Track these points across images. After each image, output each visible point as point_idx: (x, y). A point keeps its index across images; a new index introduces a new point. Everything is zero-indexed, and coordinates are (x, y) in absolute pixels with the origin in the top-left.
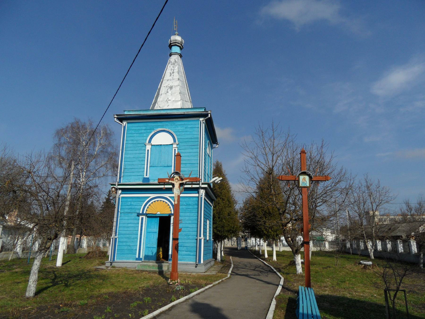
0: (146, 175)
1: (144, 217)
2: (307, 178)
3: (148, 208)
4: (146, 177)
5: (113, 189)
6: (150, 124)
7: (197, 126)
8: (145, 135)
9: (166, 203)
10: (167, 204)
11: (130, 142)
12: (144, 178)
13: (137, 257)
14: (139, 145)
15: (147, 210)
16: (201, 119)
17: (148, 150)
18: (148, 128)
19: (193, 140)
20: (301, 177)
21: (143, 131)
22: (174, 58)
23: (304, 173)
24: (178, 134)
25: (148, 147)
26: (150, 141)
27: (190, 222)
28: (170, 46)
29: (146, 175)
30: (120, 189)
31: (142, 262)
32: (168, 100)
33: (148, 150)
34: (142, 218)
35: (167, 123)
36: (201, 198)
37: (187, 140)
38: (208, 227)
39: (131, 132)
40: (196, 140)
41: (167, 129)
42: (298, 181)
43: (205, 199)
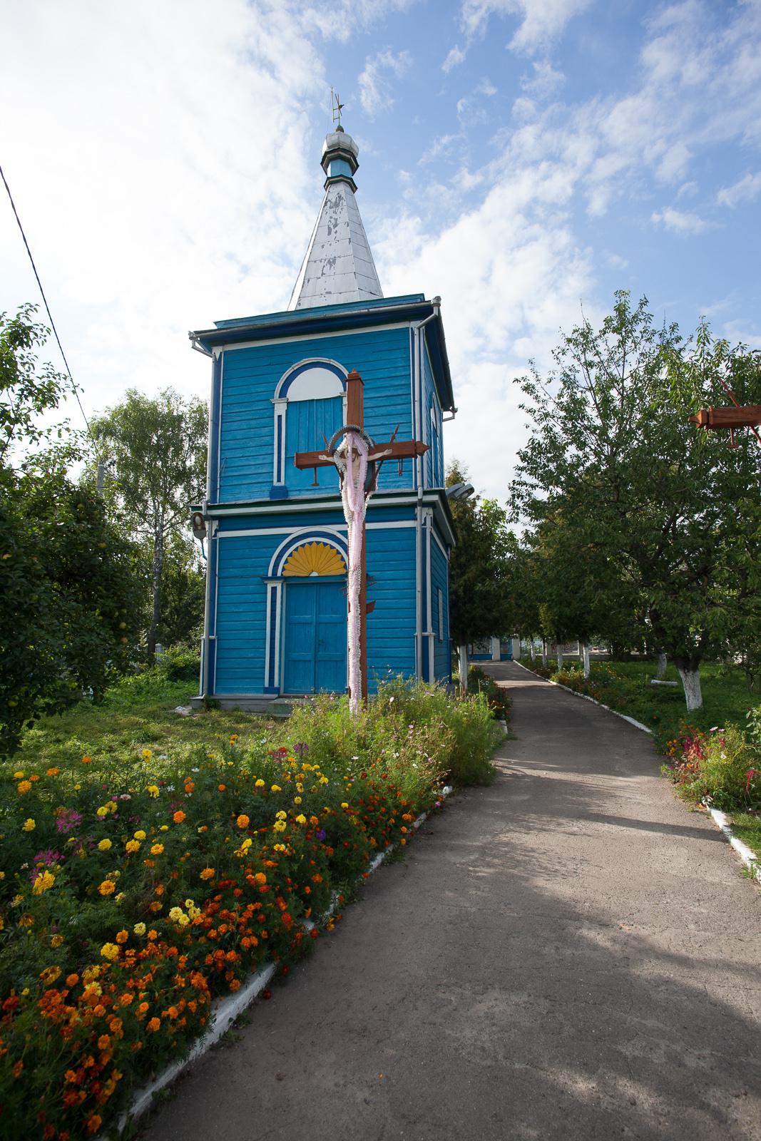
0: (279, 480)
3: (286, 562)
4: (279, 484)
5: (197, 518)
9: (332, 547)
10: (334, 551)
13: (267, 685)
15: (284, 569)
16: (415, 325)
17: (280, 417)
25: (281, 409)
26: (283, 394)
29: (279, 480)
30: (214, 518)
31: (279, 697)
33: (280, 417)
34: (274, 589)
36: (424, 531)
38: (441, 618)
43: (431, 533)
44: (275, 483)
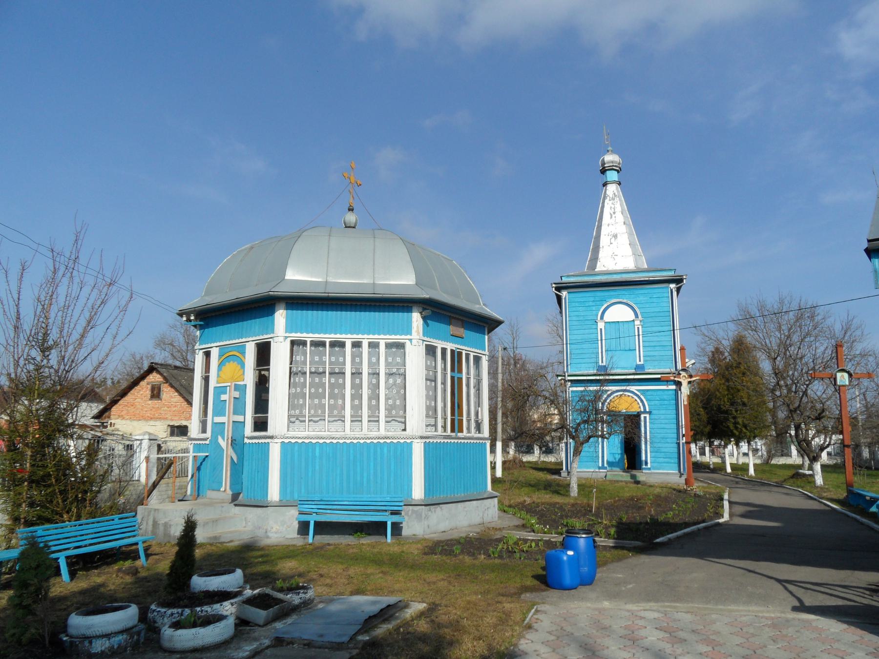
1: (647, 416)
2: (846, 375)
6: (600, 293)
7: (666, 295)
8: (594, 308)
11: (574, 318)
12: (599, 366)
14: (587, 322)
18: (597, 299)
19: (662, 314)
20: (839, 375)
21: (591, 304)
22: (612, 189)
23: (843, 370)
24: (641, 306)
25: (601, 325)
26: (602, 318)
27: (666, 421)
28: (603, 171)
32: (614, 256)
34: (645, 418)
35: (624, 292)
37: (653, 315)
39: (573, 304)
40: (667, 314)
41: (625, 301)
42: (835, 379)
44: (638, 363)
